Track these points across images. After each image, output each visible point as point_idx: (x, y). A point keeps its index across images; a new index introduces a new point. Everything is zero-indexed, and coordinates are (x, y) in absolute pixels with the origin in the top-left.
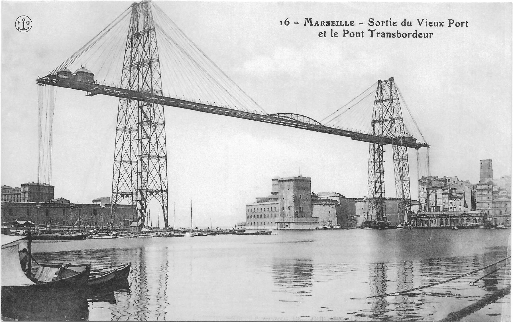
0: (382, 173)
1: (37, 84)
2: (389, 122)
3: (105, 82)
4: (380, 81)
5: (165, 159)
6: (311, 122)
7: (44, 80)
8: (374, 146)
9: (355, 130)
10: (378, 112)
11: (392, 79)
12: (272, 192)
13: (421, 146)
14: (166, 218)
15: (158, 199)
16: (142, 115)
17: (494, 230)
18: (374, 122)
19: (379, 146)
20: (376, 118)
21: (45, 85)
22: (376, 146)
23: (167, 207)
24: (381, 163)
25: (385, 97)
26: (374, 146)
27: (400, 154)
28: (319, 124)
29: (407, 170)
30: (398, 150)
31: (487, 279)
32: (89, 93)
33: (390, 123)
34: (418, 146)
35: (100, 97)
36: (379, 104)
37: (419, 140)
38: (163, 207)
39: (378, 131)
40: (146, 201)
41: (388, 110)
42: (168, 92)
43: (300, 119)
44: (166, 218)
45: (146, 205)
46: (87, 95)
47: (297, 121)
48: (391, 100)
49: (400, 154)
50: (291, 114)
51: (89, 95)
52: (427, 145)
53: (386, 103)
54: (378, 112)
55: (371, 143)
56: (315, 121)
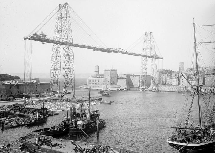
25: (148, 40)
42: (75, 42)
43: (120, 50)
46: (42, 43)
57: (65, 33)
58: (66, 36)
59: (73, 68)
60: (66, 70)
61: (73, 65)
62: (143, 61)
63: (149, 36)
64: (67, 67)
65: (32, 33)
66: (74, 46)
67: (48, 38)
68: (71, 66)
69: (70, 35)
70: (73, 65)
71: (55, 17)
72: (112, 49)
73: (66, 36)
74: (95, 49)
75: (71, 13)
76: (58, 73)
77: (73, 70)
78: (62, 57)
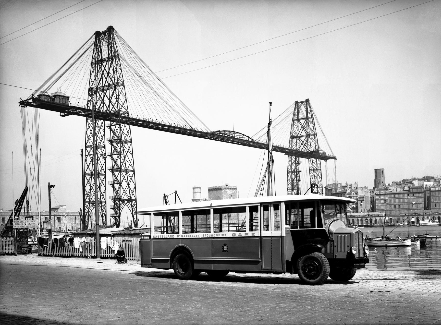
0: (298, 181)
1: (19, 105)
2: (305, 138)
3: (79, 104)
4: (297, 102)
5: (133, 172)
6: (246, 138)
7: (25, 102)
8: (291, 158)
9: (279, 145)
10: (295, 129)
11: (308, 100)
12: (192, 199)
13: (329, 158)
14: (136, 223)
15: (128, 206)
16: (264, 134)
17: (35, 258)
18: (292, 137)
19: (296, 159)
20: (294, 134)
21: (27, 107)
22: (294, 159)
23: (106, 216)
24: (298, 173)
25: (301, 116)
26: (291, 158)
27: (315, 165)
28: (251, 140)
29: (321, 179)
30: (313, 162)
31: (303, 274)
32: (62, 114)
33: (306, 139)
34: (325, 158)
35: (72, 118)
36: (296, 122)
37: (328, 153)
38: (132, 214)
39: (296, 145)
40: (120, 209)
41: (304, 127)
42: (134, 114)
43: (236, 136)
44: (136, 223)
45: (120, 212)
46: (61, 116)
47: (233, 138)
48: (307, 119)
49: (315, 165)
50: (230, 131)
51: (63, 116)
52: (335, 158)
53: (302, 122)
54: (295, 129)
55: (289, 156)
56: (248, 137)
57: (111, 93)
58: (114, 100)
59: (130, 168)
60: (116, 173)
61: (132, 162)
62: (292, 164)
63: (303, 108)
64: (117, 166)
65: (37, 91)
66: (133, 124)
67: (73, 102)
68: (127, 165)
69: (122, 98)
70: (132, 162)
71: (88, 58)
72: (228, 133)
73: (114, 100)
74: (325, 137)
75: (121, 50)
76: (126, 177)
77: (131, 173)
78: (108, 145)
